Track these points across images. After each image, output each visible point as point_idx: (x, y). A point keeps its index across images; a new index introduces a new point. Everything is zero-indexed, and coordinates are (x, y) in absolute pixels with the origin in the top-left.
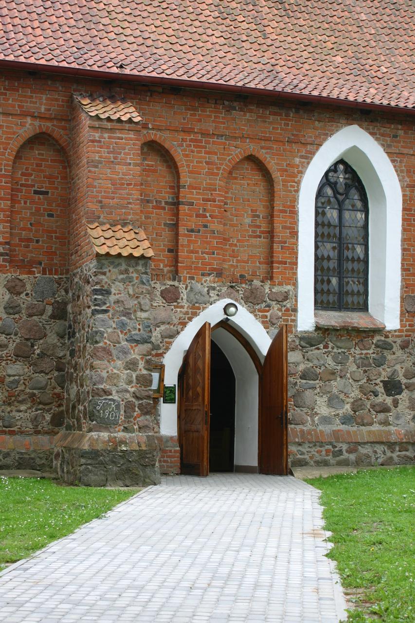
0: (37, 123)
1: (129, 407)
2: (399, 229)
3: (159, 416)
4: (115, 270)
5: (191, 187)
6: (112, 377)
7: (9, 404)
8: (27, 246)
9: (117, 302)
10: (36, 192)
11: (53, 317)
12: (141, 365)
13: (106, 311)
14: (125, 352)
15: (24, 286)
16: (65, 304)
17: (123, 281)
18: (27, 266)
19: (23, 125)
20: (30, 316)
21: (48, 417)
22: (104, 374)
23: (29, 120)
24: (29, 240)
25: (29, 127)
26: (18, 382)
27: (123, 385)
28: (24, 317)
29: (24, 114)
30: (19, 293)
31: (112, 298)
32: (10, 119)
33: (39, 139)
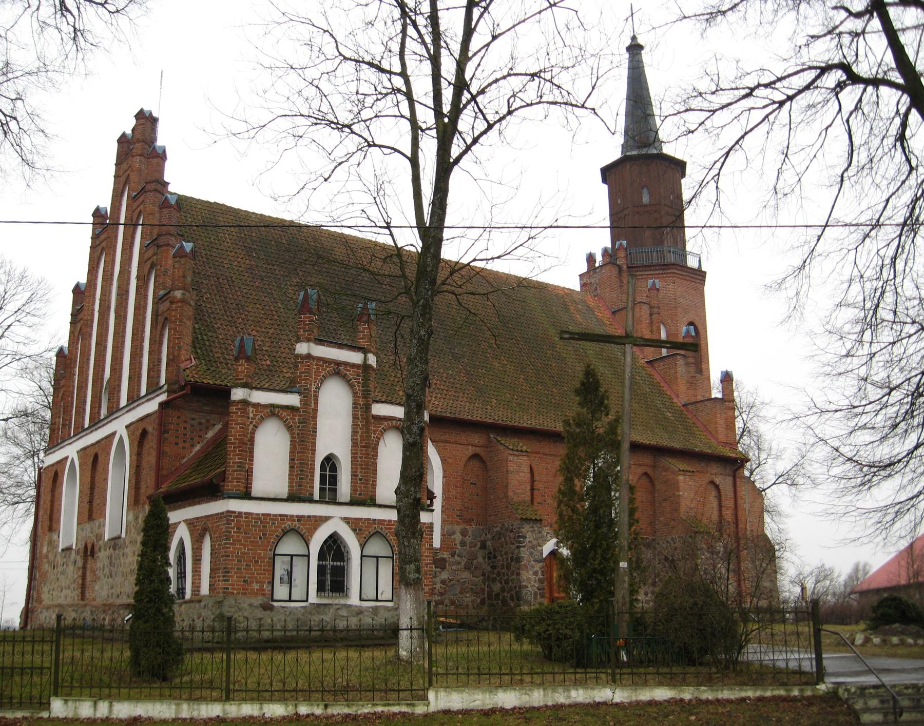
0: (474, 448)
1: (535, 594)
2: (441, 475)
3: (8, 628)
4: (528, 526)
5: (539, 481)
6: (529, 579)
7: (462, 593)
8: (467, 511)
9: (529, 542)
10: (471, 483)
11: (481, 548)
12: (540, 573)
13: (524, 546)
14: (533, 567)
15: (468, 532)
16: (485, 541)
17: (531, 531)
18: (469, 522)
19: (468, 450)
20: (470, 547)
21: (479, 601)
22: (525, 578)
23: (470, 447)
24: (468, 508)
25: (470, 451)
26: (465, 582)
27: (533, 583)
28: (468, 548)
29: (468, 445)
30: (466, 536)
31: (527, 540)
32: (747, 506)
33: (475, 456)
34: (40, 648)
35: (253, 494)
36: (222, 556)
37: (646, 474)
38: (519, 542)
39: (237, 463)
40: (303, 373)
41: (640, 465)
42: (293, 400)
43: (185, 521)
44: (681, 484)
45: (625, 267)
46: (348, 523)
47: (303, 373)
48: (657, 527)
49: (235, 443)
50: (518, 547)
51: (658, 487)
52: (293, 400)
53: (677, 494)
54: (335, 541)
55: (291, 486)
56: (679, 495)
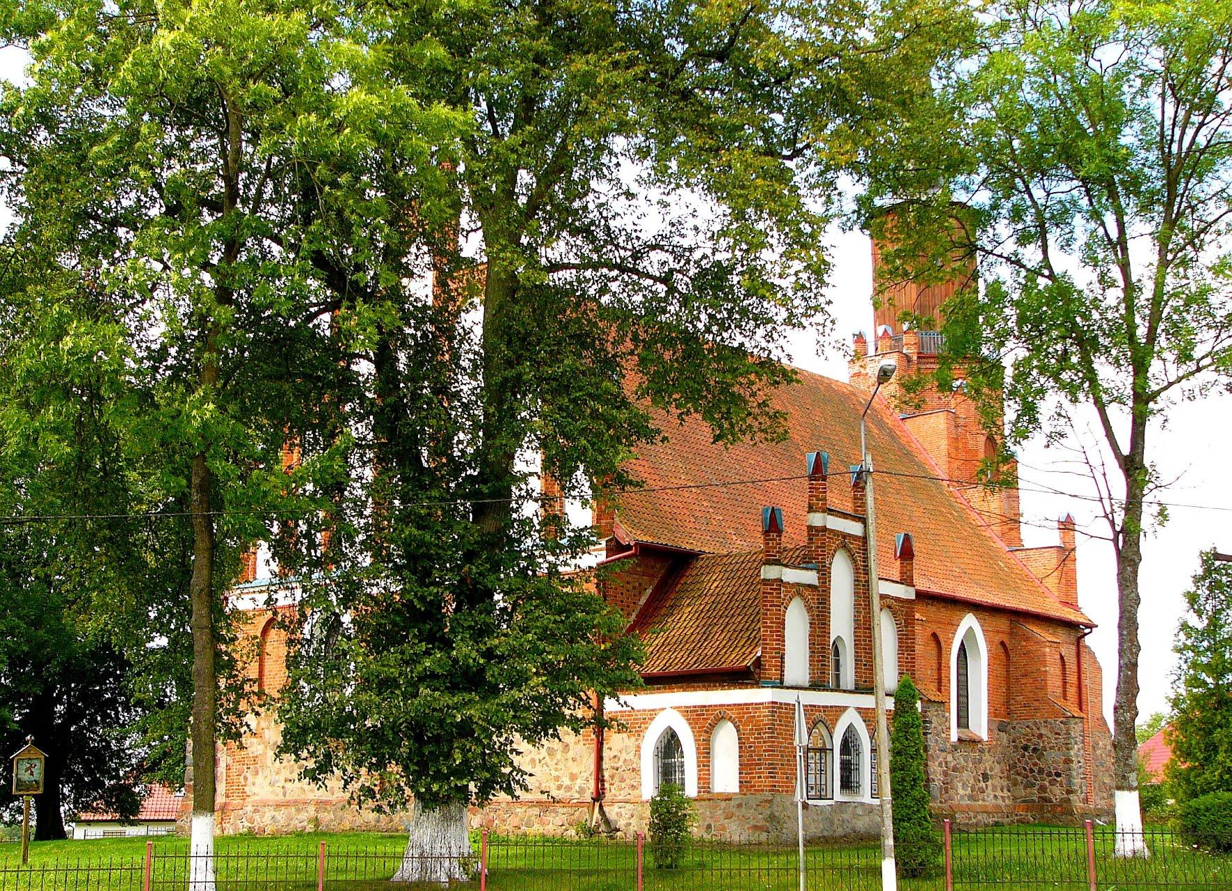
34: (573, 863)
35: (786, 683)
36: (764, 751)
37: (1002, 643)
38: (925, 728)
39: (775, 649)
40: (818, 547)
41: (998, 632)
42: (810, 577)
43: (857, 709)
44: (1048, 658)
45: (915, 358)
46: (860, 713)
47: (818, 547)
48: (1012, 707)
49: (772, 627)
50: (925, 734)
51: (1014, 658)
52: (810, 577)
53: (1043, 669)
54: (852, 728)
55: (812, 674)
56: (1046, 671)
